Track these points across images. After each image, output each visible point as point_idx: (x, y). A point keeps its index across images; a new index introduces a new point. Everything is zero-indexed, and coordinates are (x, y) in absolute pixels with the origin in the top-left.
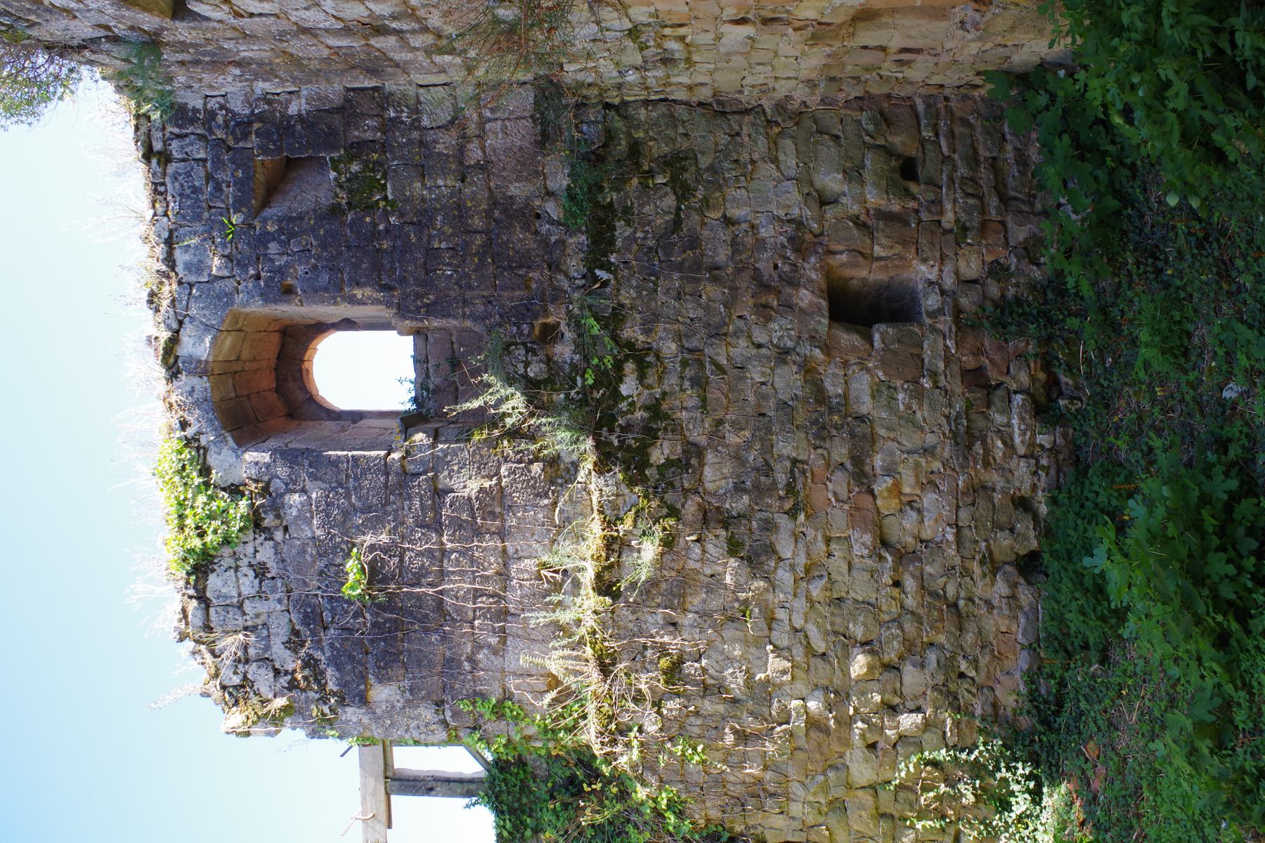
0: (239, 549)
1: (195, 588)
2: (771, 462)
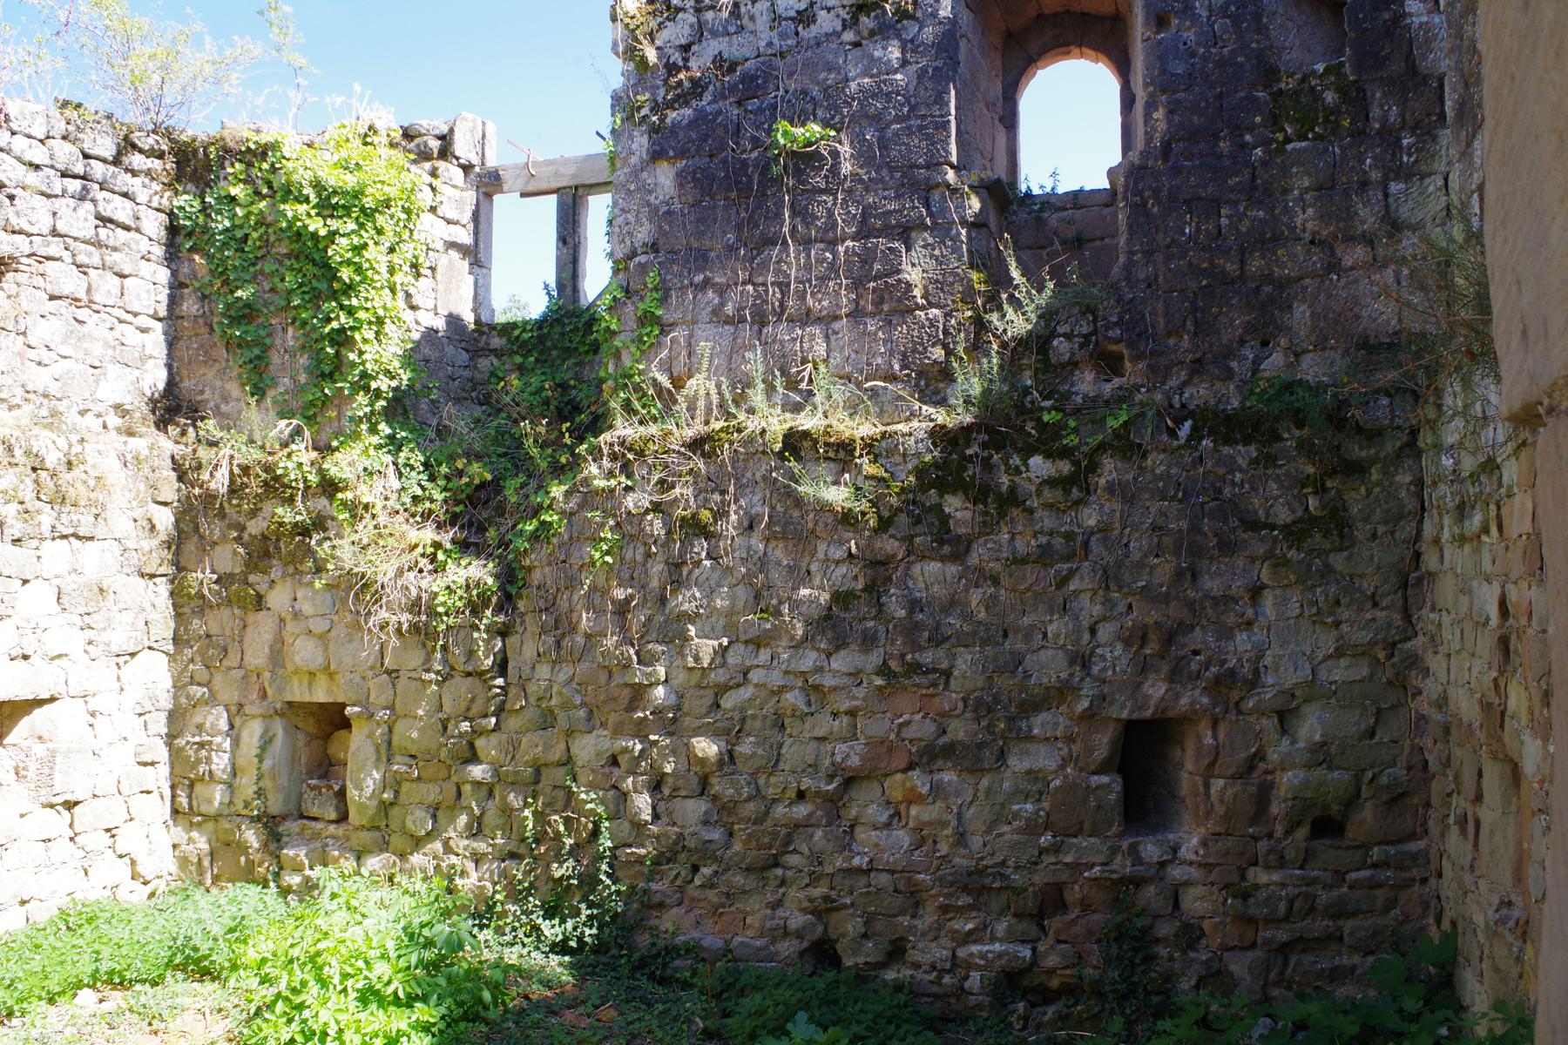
2: (947, 645)
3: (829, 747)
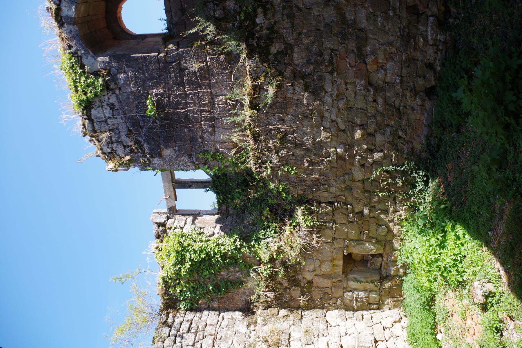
0: (102, 98)
1: (87, 115)
2: (322, 50)
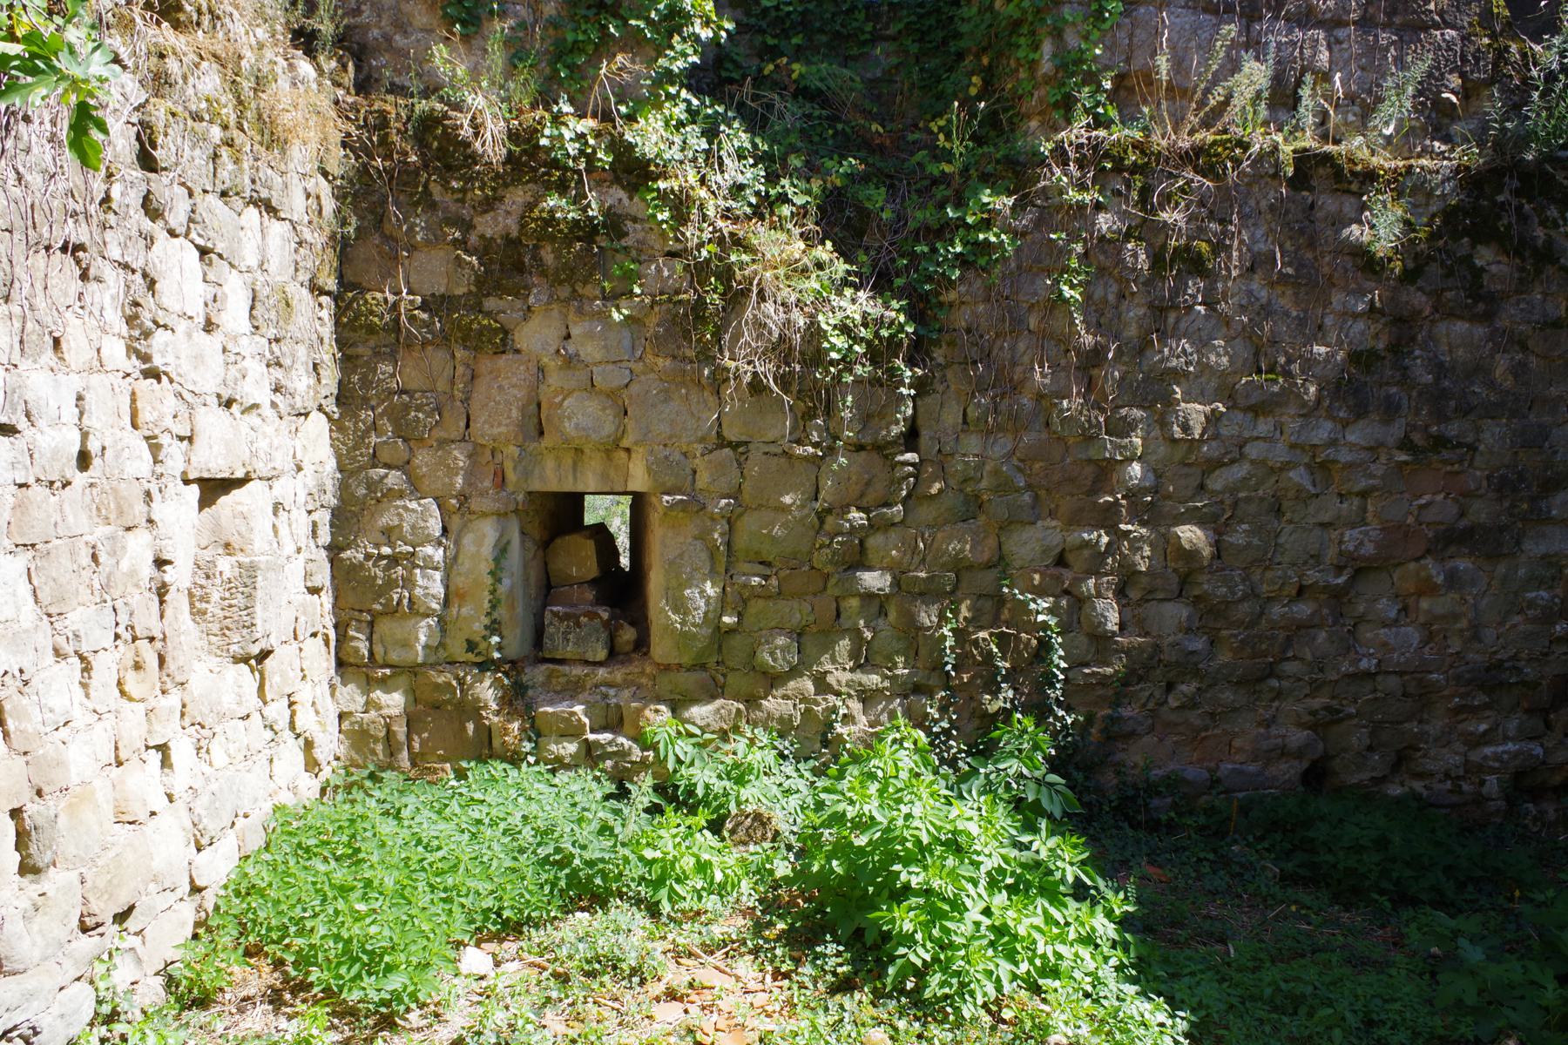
2: (1472, 417)
3: (1335, 535)
